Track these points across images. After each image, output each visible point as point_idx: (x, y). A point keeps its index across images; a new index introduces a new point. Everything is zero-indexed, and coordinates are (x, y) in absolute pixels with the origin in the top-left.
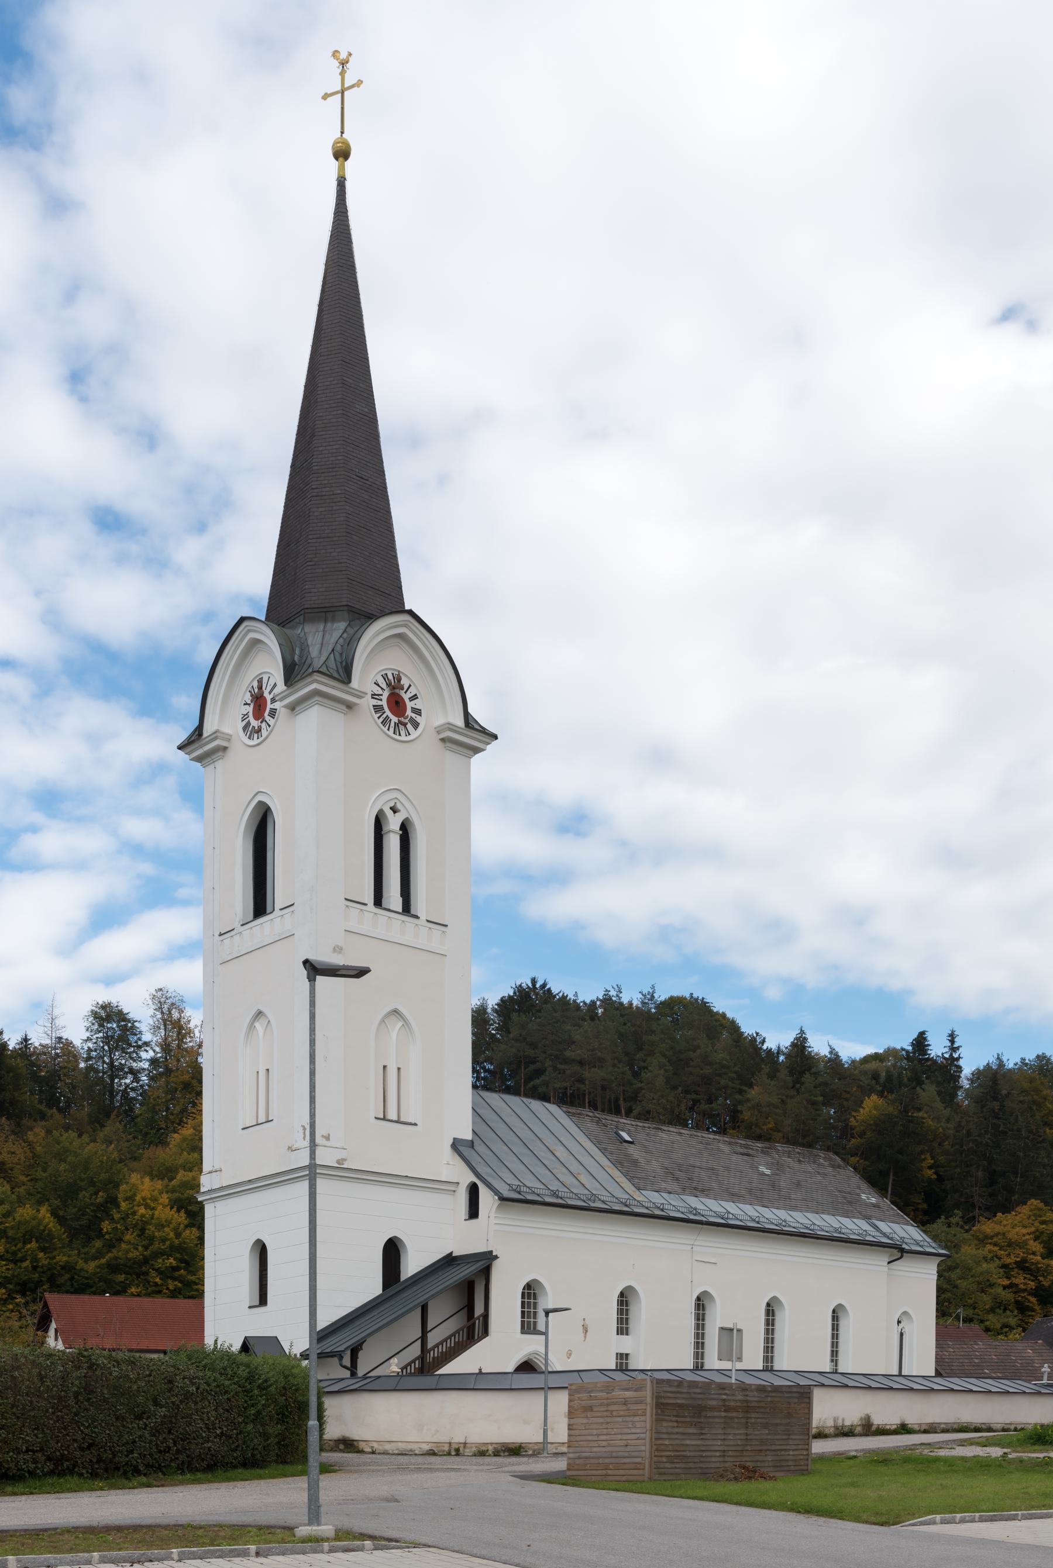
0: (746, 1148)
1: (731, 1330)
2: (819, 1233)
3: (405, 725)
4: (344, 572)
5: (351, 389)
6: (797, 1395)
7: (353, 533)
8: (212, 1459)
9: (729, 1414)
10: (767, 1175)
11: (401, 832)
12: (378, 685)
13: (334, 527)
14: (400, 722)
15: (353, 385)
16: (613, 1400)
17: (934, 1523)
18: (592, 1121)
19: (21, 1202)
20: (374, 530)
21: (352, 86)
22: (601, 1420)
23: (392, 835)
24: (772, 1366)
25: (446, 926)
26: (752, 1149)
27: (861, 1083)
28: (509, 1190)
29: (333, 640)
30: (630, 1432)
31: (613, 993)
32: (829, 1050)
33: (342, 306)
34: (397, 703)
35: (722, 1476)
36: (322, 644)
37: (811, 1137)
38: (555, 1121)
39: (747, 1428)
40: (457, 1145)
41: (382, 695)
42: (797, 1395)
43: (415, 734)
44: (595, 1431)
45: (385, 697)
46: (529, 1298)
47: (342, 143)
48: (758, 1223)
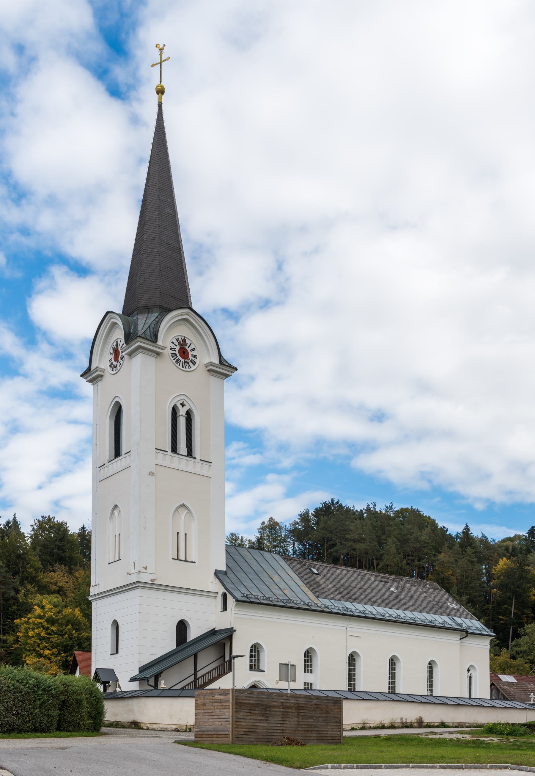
0: (384, 578)
1: (287, 665)
2: (418, 622)
3: (188, 363)
4: (157, 289)
5: (163, 202)
6: (332, 701)
7: (163, 270)
8: (10, 727)
9: (286, 710)
10: (395, 592)
11: (186, 416)
12: (174, 344)
13: (153, 268)
14: (185, 362)
15: (164, 200)
16: (215, 700)
17: (327, 768)
18: (298, 563)
19: (66, 606)
20: (174, 269)
21: (165, 60)
22: (209, 711)
23: (181, 417)
24: (354, 689)
25: (211, 463)
26: (388, 579)
27: (498, 552)
28: (242, 596)
29: (150, 322)
30: (222, 717)
31: (371, 506)
32: (481, 535)
33: (159, 163)
34: (184, 352)
35: (275, 743)
36: (144, 324)
37: (469, 579)
38: (276, 562)
39: (298, 718)
40: (217, 573)
41: (176, 348)
42: (332, 701)
43: (193, 368)
44: (207, 717)
45: (178, 348)
46: (352, 661)
47: (160, 86)
48: (384, 616)
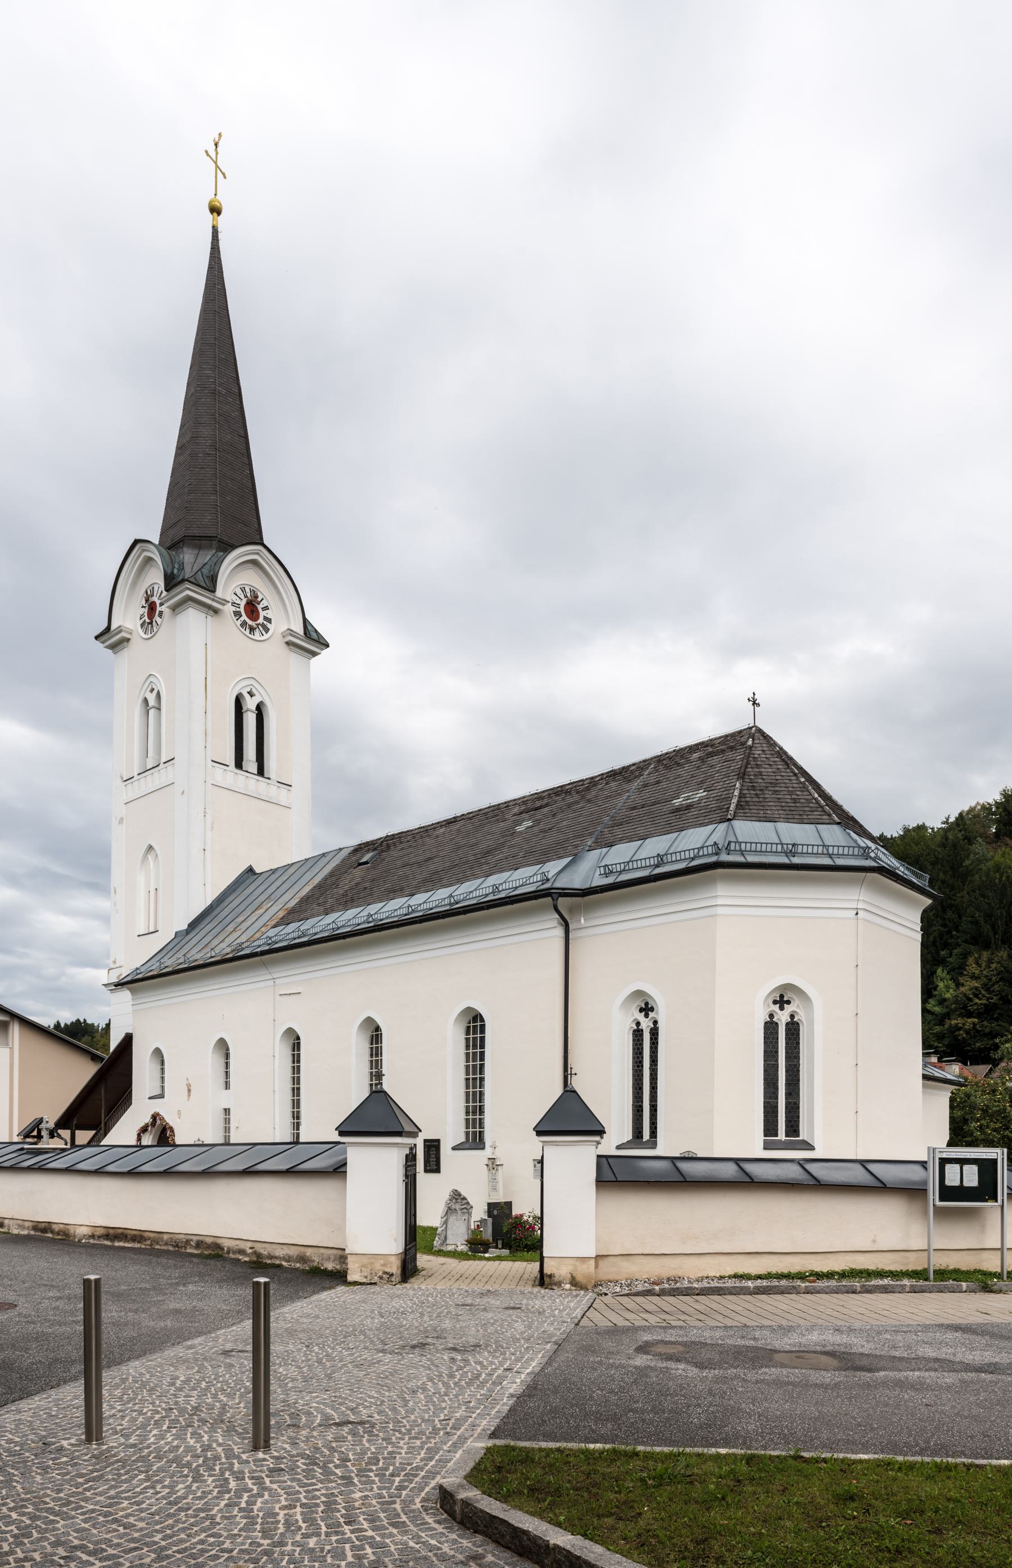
45: (243, 603)
